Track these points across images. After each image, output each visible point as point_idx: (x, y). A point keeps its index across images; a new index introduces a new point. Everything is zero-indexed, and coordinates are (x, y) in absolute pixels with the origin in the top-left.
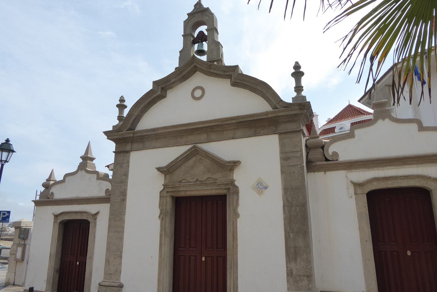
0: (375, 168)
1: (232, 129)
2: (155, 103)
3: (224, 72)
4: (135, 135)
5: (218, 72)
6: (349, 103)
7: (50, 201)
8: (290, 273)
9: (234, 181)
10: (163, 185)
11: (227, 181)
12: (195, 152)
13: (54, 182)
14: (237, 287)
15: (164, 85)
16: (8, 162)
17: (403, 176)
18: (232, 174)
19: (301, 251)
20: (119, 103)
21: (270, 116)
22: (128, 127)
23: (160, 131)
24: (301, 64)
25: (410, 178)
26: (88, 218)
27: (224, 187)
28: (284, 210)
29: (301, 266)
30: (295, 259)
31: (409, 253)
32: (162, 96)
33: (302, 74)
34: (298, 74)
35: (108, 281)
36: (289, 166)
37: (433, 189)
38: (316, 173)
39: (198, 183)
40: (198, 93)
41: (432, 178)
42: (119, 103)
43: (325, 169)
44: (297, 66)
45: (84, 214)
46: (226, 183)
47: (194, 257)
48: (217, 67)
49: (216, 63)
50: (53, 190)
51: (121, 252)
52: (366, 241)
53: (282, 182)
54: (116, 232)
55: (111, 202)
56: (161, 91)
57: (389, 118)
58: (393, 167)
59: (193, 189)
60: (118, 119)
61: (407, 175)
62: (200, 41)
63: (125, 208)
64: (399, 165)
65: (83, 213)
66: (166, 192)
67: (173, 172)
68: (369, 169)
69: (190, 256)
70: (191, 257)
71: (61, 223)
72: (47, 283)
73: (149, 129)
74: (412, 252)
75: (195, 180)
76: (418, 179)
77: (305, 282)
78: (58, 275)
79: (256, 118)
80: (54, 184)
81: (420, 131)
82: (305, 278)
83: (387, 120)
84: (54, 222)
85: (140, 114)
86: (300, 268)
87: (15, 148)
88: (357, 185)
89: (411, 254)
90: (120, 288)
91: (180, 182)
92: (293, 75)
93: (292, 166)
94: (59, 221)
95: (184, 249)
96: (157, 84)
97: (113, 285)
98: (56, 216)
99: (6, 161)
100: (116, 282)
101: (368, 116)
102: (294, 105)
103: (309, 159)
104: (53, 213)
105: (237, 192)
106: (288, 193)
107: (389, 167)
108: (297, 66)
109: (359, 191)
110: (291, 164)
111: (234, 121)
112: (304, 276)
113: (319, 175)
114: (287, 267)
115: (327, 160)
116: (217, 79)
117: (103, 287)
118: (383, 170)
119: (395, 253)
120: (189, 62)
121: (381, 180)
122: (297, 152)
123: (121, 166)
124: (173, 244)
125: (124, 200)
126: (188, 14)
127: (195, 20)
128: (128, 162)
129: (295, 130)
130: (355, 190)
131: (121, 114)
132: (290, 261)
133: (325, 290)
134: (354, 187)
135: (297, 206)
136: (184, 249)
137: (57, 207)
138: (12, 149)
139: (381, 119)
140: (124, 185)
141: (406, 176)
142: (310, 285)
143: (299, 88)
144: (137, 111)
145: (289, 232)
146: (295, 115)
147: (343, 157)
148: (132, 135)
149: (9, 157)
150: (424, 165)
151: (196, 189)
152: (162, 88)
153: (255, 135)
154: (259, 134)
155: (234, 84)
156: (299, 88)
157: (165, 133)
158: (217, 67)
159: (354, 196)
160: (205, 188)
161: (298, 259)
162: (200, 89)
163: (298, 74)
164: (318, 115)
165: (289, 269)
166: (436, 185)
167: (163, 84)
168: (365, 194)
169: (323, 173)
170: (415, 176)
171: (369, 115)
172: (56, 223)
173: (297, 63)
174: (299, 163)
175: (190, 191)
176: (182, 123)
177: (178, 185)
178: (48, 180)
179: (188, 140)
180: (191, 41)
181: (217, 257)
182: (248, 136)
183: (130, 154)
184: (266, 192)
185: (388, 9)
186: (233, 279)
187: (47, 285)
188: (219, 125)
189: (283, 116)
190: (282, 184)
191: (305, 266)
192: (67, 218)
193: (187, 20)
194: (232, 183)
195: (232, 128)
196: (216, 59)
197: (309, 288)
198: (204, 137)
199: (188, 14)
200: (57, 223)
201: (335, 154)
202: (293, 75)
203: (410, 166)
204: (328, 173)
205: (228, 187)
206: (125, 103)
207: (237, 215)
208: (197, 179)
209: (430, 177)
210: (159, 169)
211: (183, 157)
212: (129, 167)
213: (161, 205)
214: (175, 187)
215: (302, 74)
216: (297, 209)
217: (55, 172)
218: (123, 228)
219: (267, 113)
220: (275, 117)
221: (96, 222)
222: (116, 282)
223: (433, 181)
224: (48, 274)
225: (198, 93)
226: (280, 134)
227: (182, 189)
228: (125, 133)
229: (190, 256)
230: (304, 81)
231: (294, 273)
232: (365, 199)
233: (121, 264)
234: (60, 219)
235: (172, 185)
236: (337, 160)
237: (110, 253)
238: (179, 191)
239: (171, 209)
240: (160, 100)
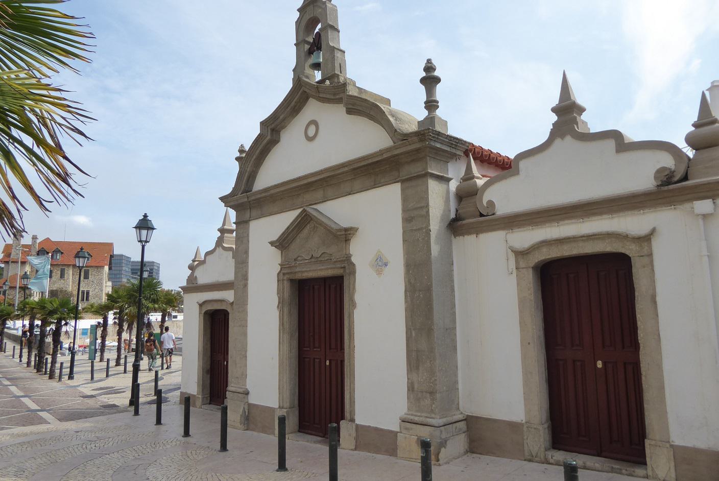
0: (547, 225)
1: (349, 180)
2: (269, 152)
3: (335, 94)
4: (249, 200)
5: (328, 96)
7: (196, 287)
8: (411, 388)
9: (350, 257)
10: (279, 264)
11: (342, 256)
12: (304, 221)
13: (198, 262)
14: (354, 402)
15: (273, 126)
16: (148, 242)
17: (586, 235)
18: (348, 245)
19: (424, 357)
20: (424, 74)
21: (385, 156)
22: (242, 189)
23: (272, 192)
24: (434, 62)
25: (597, 239)
27: (339, 266)
28: (406, 296)
29: (424, 378)
30: (417, 368)
31: (600, 364)
32: (274, 141)
33: (437, 80)
34: (430, 80)
35: (235, 385)
36: (412, 230)
37: (634, 257)
38: (466, 237)
39: (313, 260)
40: (312, 131)
41: (630, 237)
42: (424, 74)
43: (477, 230)
44: (429, 68)
46: (342, 259)
47: (318, 360)
48: (325, 89)
49: (328, 82)
50: (198, 273)
51: (246, 351)
52: (529, 343)
53: (404, 256)
54: (240, 326)
55: (235, 288)
56: (272, 134)
57: (571, 135)
58: (573, 221)
59: (308, 269)
60: (425, 107)
61: (591, 234)
62: (315, 48)
63: (247, 296)
64: (582, 217)
66: (282, 275)
67: (288, 245)
68: (537, 226)
69: (314, 359)
70: (316, 360)
71: (206, 313)
74: (604, 364)
75: (310, 257)
76: (609, 240)
77: (428, 402)
78: (209, 376)
79: (370, 161)
80: (198, 265)
81: (619, 152)
82: (428, 395)
83: (568, 138)
85: (254, 169)
86: (422, 380)
87: (155, 224)
88: (520, 254)
89: (602, 365)
90: (244, 395)
91: (295, 260)
92: (423, 81)
93: (415, 230)
94: (203, 312)
95: (308, 349)
96: (265, 126)
98: (201, 305)
99: (146, 242)
100: (242, 388)
102: (410, 135)
103: (459, 214)
104: (197, 302)
105: (354, 272)
106: (411, 272)
107: (566, 222)
108: (429, 68)
109: (522, 264)
110: (415, 228)
111: (346, 169)
112: (426, 392)
113: (470, 239)
114: (408, 379)
115: (481, 215)
116: (331, 105)
118: (558, 226)
119: (578, 363)
120: (296, 86)
121: (553, 243)
122: (422, 208)
123: (242, 241)
124: (295, 343)
125: (246, 285)
126: (298, 10)
127: (307, 17)
128: (248, 235)
129: (420, 173)
130: (517, 262)
131: (431, 97)
132: (411, 371)
133: (474, 415)
134: (516, 257)
135: (420, 291)
137: (199, 294)
138: (150, 226)
139: (559, 137)
140: (245, 266)
141: (590, 236)
142: (433, 406)
143: (431, 105)
144: (250, 166)
145: (410, 329)
146: (418, 150)
147: (503, 208)
148: (246, 200)
150: (621, 214)
151: (311, 269)
152: (273, 130)
153: (375, 186)
154: (380, 183)
155: (350, 111)
156: (431, 105)
157: (279, 192)
158: (325, 89)
159: (515, 270)
160: (320, 268)
161: (420, 368)
162: (312, 124)
163: (430, 80)
165: (410, 382)
166: (637, 248)
167: (271, 124)
168: (529, 267)
169: (475, 236)
170: (604, 234)
173: (429, 61)
174: (424, 226)
175: (306, 271)
176: (292, 178)
177: (293, 264)
178: (194, 261)
179: (305, 200)
180: (306, 50)
181: (625, 364)
183: (249, 224)
184: (386, 270)
185: (9, 228)
186: (349, 391)
188: (333, 176)
189: (401, 154)
190: (404, 258)
191: (428, 379)
193: (299, 17)
194: (348, 258)
195: (350, 178)
196: (329, 75)
197: (432, 409)
198: (319, 194)
199: (298, 10)
201: (491, 204)
202: (423, 81)
203: (600, 217)
204: (483, 236)
205: (343, 266)
206: (436, 73)
207: (354, 305)
208: (312, 255)
210: (272, 243)
211: (293, 226)
212: (249, 242)
213: (280, 292)
214: (291, 267)
215: (437, 80)
216: (421, 296)
217: (200, 248)
218: (247, 321)
219: (388, 150)
220: (391, 157)
222: (242, 388)
223: (634, 243)
225: (312, 131)
226: (403, 181)
227: (298, 269)
228: (239, 197)
229: (314, 359)
230: (440, 91)
231: (416, 386)
232: (529, 277)
234: (205, 309)
235: (288, 264)
236: (493, 214)
239: (289, 296)
240: (274, 146)
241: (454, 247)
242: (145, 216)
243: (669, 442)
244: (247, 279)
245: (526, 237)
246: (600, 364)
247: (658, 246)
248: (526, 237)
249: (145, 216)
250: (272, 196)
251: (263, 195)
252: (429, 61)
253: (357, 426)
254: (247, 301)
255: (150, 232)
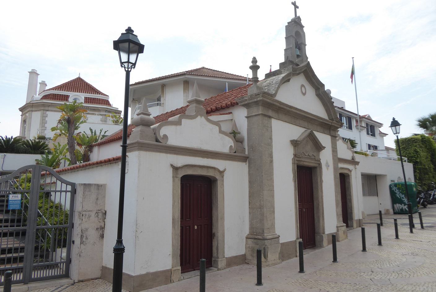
6: (79, 76)
20: (251, 64)
26: (215, 175)
31: (196, 227)
42: (251, 64)
44: (254, 61)
45: (210, 170)
51: (274, 208)
54: (269, 190)
65: (209, 169)
72: (173, 257)
73: (289, 105)
84: (173, 177)
88: (175, 169)
94: (180, 176)
97: (272, 238)
101: (101, 95)
108: (254, 61)
115: (157, 141)
117: (268, 240)
136: (189, 219)
147: (172, 141)
149: (397, 129)
164: (38, 75)
171: (102, 95)
172: (177, 177)
173: (254, 58)
182: (303, 126)
187: (173, 261)
192: (190, 172)
200: (178, 178)
201: (165, 137)
202: (251, 68)
209: (344, 168)
218: (273, 186)
221: (223, 180)
224: (173, 245)
233: (274, 218)
234: (181, 174)
237: (267, 209)
238: (301, 161)
241: (41, 157)
242: (394, 119)
243: (296, 241)
244: (272, 157)
245: (181, 160)
246: (196, 227)
247: (226, 175)
248: (181, 160)
249: (394, 119)
250: (288, 111)
251: (288, 109)
252: (254, 58)
253: (226, 258)
254: (273, 172)
255: (397, 127)
